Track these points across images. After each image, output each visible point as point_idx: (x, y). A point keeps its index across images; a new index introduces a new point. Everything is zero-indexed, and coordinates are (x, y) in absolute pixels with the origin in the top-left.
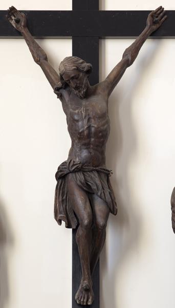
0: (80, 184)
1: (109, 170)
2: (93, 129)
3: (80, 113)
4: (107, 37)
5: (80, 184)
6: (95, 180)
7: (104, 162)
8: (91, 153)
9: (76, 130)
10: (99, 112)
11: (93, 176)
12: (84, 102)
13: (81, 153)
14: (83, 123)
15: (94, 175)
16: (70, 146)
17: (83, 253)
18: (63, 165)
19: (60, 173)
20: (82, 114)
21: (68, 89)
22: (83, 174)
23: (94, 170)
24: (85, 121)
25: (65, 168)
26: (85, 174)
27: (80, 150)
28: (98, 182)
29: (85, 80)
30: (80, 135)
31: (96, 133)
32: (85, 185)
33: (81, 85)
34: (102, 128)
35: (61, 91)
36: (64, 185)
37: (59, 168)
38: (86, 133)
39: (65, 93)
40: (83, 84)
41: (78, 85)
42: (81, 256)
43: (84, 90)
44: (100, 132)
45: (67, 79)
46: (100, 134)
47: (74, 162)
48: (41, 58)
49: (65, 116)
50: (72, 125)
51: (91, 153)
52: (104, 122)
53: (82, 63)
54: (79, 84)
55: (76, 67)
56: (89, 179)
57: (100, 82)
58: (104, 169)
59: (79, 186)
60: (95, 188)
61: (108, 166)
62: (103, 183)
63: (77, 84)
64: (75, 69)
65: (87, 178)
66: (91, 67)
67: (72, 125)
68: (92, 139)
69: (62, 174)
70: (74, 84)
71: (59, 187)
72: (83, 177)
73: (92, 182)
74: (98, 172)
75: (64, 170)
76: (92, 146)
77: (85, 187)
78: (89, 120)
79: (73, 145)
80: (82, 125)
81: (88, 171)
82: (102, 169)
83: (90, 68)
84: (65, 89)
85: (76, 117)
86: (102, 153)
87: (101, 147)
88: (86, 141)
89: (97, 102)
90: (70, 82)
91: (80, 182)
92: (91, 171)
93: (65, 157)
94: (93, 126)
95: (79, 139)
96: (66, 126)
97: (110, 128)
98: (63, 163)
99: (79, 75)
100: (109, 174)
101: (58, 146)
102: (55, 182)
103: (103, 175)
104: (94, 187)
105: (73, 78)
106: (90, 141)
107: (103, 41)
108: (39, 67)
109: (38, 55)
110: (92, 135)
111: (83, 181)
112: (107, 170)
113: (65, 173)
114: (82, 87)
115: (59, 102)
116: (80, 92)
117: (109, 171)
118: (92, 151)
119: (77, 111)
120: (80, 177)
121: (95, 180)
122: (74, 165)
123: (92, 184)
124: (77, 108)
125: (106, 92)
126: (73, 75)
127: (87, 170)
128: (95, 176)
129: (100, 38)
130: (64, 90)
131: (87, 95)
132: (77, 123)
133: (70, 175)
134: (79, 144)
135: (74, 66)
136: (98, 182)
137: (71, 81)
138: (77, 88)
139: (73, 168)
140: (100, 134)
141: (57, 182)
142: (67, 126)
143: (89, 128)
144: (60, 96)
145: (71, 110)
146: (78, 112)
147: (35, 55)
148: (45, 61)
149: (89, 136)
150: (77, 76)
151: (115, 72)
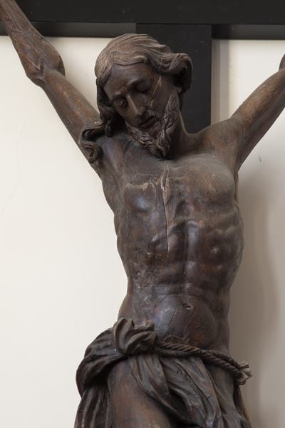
0: (151, 389)
1: (241, 363)
2: (193, 236)
3: (155, 191)
4: (242, 28)
5: (151, 389)
6: (196, 382)
7: (225, 341)
8: (184, 305)
9: (140, 239)
10: (210, 187)
11: (190, 370)
12: (167, 166)
13: (155, 306)
14: (162, 217)
15: (195, 368)
16: (122, 292)
18: (102, 341)
19: (91, 365)
20: (160, 192)
21: (119, 137)
22: (163, 366)
23: (195, 355)
24: (170, 214)
25: (107, 346)
26: (167, 363)
27: (154, 294)
28: (208, 389)
29: (171, 102)
30: (155, 251)
31: (203, 244)
32: (167, 393)
34: (220, 231)
35: (100, 142)
36: (102, 408)
37: (88, 351)
38: (171, 242)
39: (111, 149)
40: (164, 112)
41: (151, 113)
43: (169, 130)
44: (216, 241)
45: (118, 93)
46: (215, 250)
47: (133, 324)
48: (46, 73)
49: (108, 215)
50: (131, 228)
51: (184, 305)
52: (224, 216)
53: (162, 50)
54: (155, 109)
56: (178, 379)
57: (213, 123)
58: (226, 359)
59: (148, 395)
60: (198, 403)
61: (235, 351)
62: (219, 392)
63: (147, 108)
64: (141, 62)
65: (172, 375)
66: (187, 62)
67: (131, 228)
68: (191, 265)
69: (97, 366)
70: (139, 107)
71: (86, 410)
72: (160, 369)
73: (189, 388)
74: (207, 363)
75: (103, 353)
76: (188, 286)
77: (167, 399)
78: (181, 208)
79: (132, 273)
80: (160, 224)
81: (180, 357)
82: (214, 354)
84: (112, 134)
85: (142, 204)
86: (220, 310)
87: (217, 293)
88: (171, 270)
89: (206, 167)
90: (126, 105)
91: (152, 382)
92: (187, 357)
93: (109, 320)
94: (192, 226)
95: (152, 262)
96: (113, 237)
97: (241, 238)
98: (102, 334)
99: (152, 81)
100: (241, 376)
101: (88, 286)
102: (74, 399)
103: (221, 376)
104: (193, 402)
105: (135, 89)
106: (183, 268)
107: (222, 44)
108: (39, 91)
109: (37, 57)
110: (191, 251)
111: (159, 381)
112: (233, 363)
113: (107, 360)
114: (160, 120)
116: (154, 135)
117: (240, 368)
118: (188, 299)
119: (145, 186)
120: (151, 368)
121: (196, 382)
122: (132, 332)
123: (189, 393)
124: (147, 179)
125: (233, 147)
126: (134, 79)
127: (173, 352)
128: (197, 370)
129: (225, 33)
131: (174, 150)
132: (145, 219)
133: (122, 366)
134: (149, 281)
135: (138, 53)
136: (208, 389)
137: (129, 97)
138: (146, 122)
139: (131, 341)
140: (215, 250)
141: (78, 399)
142: (115, 237)
143: (181, 229)
144: (97, 159)
145: (128, 185)
146: (149, 187)
147: (30, 57)
148: (56, 72)
149: (181, 253)
150: (148, 83)
151: (258, 99)
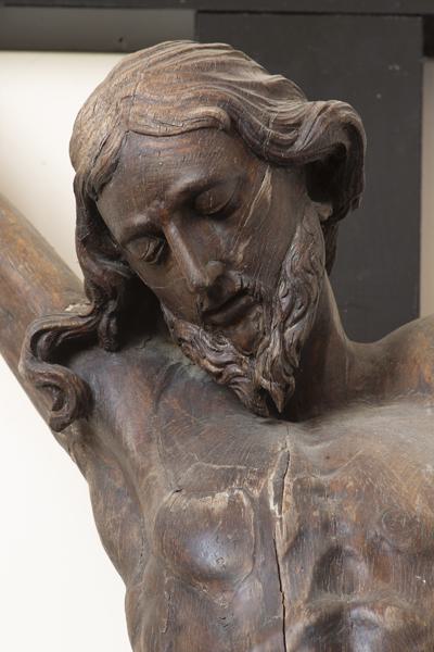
3: (250, 516)
12: (286, 440)
14: (273, 598)
17: (305, 577)
18: (139, 437)
20: (266, 520)
21: (144, 351)
24: (296, 585)
29: (299, 247)
33: (262, 285)
35: (83, 365)
40: (278, 276)
41: (238, 279)
42: (281, 552)
43: (293, 332)
50: (177, 628)
53: (275, 91)
54: (250, 268)
55: (224, 103)
63: (228, 264)
64: (209, 126)
66: (351, 129)
70: (201, 261)
78: (329, 567)
83: (341, 138)
84: (120, 343)
90: (163, 255)
94: (365, 623)
99: (244, 183)
105: (192, 206)
114: (265, 300)
115: (57, 483)
116: (250, 348)
119: (219, 501)
124: (227, 479)
126: (188, 178)
130: (115, 360)
131: (306, 395)
132: (220, 600)
135: (202, 100)
137: (172, 231)
138: (225, 307)
144: (76, 418)
146: (234, 504)
150: (230, 192)
